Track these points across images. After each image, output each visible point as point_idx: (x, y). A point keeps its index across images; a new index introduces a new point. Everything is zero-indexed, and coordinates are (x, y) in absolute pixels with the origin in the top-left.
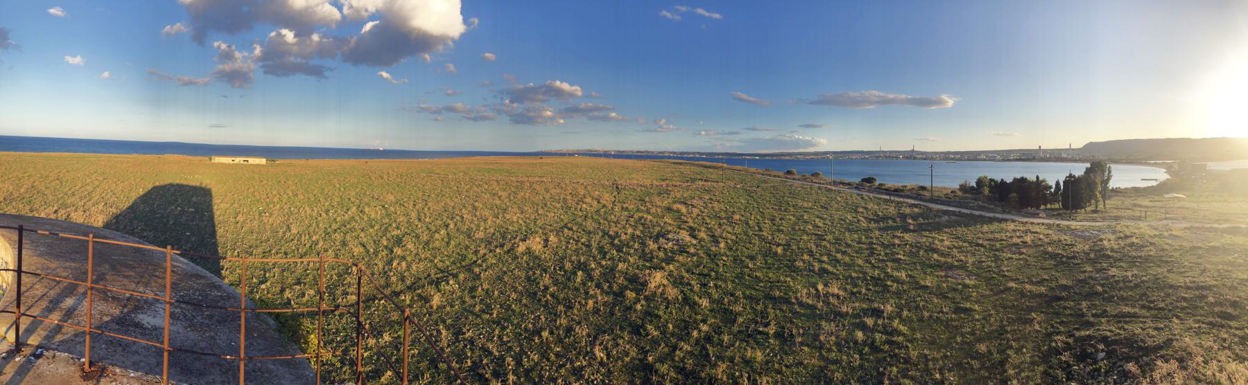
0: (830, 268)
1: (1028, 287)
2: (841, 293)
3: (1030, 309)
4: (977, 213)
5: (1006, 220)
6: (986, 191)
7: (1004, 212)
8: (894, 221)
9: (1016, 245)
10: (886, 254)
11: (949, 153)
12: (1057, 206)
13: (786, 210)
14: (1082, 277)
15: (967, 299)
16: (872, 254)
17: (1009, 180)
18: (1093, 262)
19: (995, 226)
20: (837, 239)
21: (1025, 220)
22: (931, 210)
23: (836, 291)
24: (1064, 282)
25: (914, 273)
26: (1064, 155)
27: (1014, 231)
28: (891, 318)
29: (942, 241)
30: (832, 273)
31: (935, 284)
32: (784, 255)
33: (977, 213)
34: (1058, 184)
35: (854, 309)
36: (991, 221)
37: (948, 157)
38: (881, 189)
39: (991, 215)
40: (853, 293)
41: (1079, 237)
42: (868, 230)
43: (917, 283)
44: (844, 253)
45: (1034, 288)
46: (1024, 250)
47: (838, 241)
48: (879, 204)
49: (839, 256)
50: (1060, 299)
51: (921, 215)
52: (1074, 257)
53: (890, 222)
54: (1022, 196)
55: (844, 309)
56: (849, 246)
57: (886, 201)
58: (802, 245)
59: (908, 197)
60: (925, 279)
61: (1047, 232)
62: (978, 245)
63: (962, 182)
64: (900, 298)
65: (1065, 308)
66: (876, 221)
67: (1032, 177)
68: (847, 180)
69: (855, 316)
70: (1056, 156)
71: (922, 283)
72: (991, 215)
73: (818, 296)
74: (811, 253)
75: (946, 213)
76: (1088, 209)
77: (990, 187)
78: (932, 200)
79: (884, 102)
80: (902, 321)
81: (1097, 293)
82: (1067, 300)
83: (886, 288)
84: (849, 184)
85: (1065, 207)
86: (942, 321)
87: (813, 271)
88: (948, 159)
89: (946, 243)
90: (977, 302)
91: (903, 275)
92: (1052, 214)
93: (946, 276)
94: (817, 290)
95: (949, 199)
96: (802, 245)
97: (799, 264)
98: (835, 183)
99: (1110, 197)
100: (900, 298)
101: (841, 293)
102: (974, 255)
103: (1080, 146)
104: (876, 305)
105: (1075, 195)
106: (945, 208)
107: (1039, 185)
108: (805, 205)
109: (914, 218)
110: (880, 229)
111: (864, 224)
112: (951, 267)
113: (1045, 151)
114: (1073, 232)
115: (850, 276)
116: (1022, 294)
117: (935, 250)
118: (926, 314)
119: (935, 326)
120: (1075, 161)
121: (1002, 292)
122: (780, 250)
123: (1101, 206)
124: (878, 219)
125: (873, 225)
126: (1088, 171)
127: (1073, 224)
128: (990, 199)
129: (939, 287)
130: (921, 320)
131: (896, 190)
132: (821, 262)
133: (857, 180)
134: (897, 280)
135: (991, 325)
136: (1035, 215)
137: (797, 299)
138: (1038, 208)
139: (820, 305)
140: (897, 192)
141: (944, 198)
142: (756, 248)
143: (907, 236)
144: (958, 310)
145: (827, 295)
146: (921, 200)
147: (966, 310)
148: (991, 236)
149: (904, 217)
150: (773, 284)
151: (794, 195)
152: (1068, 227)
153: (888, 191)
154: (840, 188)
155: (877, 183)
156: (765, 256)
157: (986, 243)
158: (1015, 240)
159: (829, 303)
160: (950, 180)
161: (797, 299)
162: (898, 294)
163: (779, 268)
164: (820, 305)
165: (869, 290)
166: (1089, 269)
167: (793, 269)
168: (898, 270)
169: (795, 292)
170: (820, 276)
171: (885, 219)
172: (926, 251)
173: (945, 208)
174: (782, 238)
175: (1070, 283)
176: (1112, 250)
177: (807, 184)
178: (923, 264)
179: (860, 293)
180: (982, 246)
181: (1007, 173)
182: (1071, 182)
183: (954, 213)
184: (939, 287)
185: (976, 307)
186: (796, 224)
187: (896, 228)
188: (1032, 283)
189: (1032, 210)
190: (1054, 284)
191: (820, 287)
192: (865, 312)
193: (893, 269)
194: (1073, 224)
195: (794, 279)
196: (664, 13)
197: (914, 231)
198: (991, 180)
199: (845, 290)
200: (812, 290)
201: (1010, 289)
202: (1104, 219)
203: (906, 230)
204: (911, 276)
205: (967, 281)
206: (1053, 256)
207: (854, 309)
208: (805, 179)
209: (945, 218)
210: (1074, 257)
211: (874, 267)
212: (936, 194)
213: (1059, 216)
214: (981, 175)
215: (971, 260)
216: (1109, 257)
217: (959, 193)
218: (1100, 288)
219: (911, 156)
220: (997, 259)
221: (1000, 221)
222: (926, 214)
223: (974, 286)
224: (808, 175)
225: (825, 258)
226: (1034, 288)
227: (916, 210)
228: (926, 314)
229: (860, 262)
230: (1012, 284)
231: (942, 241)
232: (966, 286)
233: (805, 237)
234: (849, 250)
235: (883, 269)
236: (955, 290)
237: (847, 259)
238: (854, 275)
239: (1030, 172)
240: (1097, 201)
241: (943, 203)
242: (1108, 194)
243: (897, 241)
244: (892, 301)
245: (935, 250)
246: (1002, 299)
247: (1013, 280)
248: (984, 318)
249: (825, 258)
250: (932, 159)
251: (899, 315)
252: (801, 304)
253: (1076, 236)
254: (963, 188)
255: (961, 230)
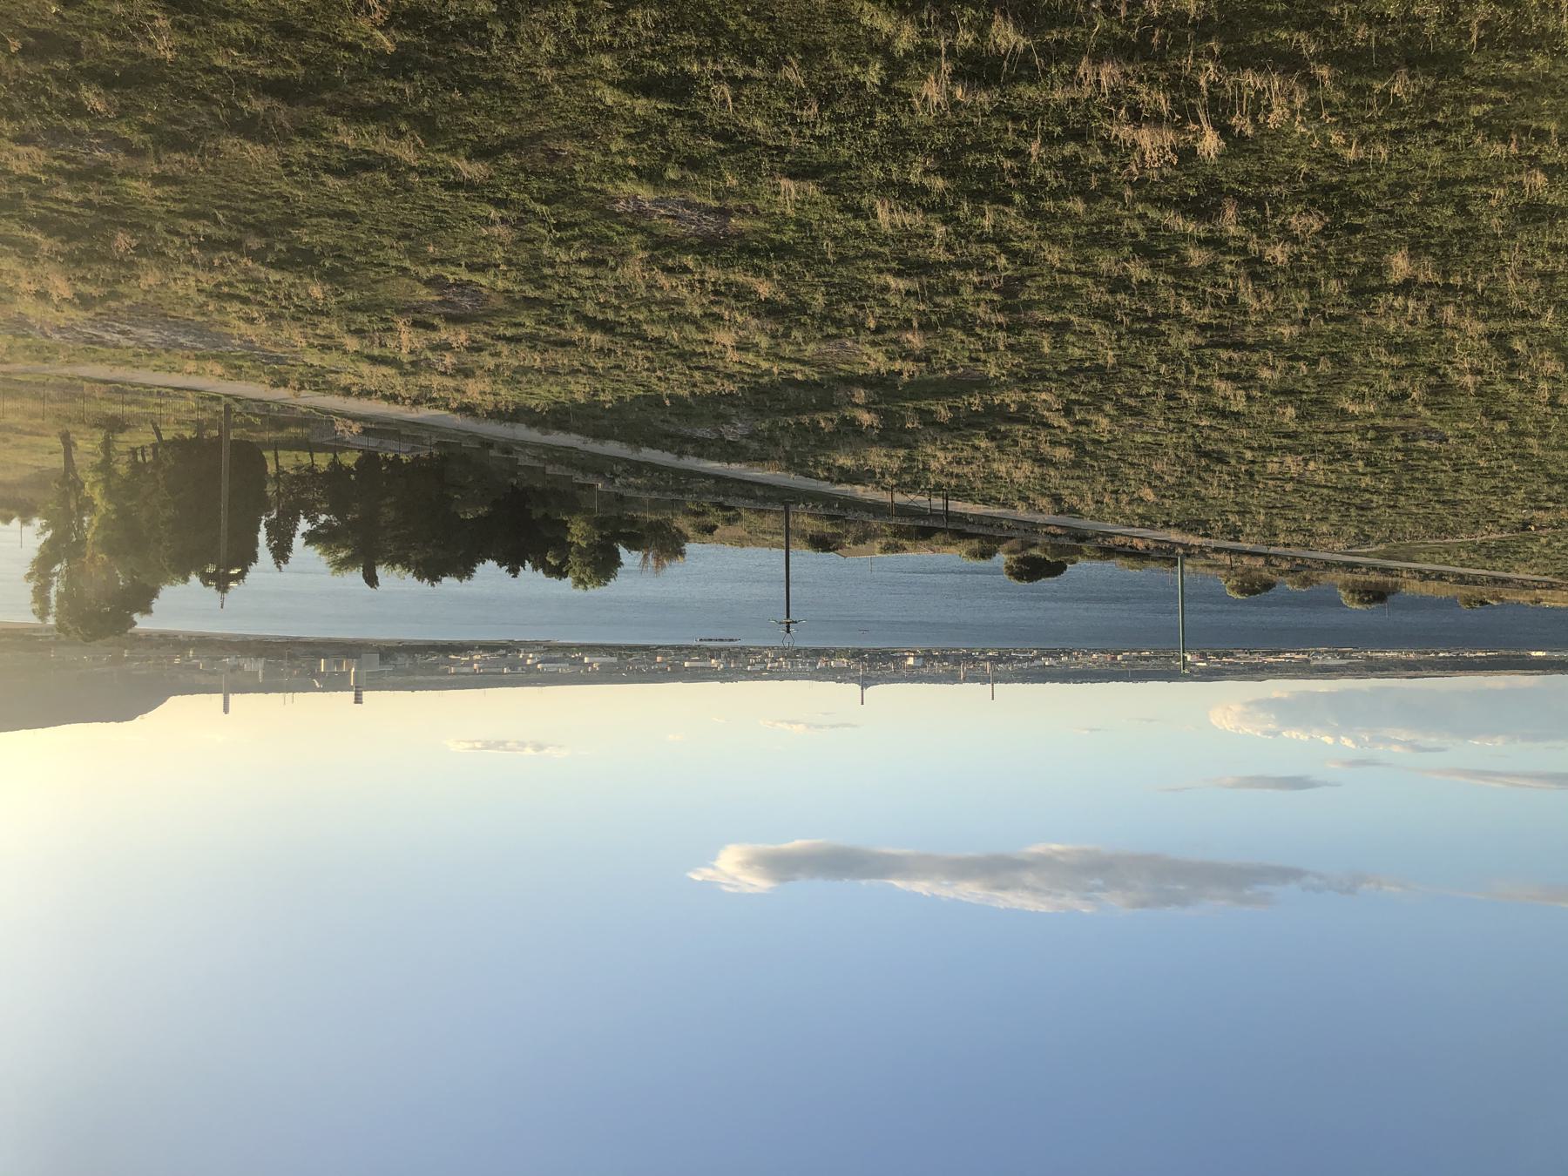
0: (1175, 221)
1: (406, 153)
2: (1125, 132)
3: (398, 65)
4: (613, 448)
5: (497, 415)
6: (578, 532)
7: (507, 447)
8: (927, 418)
9: (456, 319)
10: (953, 289)
11: (724, 676)
12: (289, 461)
13: (1382, 435)
14: (175, 162)
15: (643, 131)
16: (1009, 289)
17: (489, 572)
18: (121, 214)
19: (543, 395)
20: (1153, 335)
21: (424, 413)
22: (794, 463)
23: (1145, 138)
24: (255, 153)
25: (842, 223)
26: (255, 666)
27: (467, 373)
28: (925, 54)
29: (741, 347)
30: (1164, 203)
31: (764, 185)
32: (1378, 250)
33: (613, 448)
34: (281, 553)
35: (1071, 79)
36: (559, 417)
37: (729, 660)
38: (982, 537)
39: (558, 438)
40: (1079, 136)
41: (187, 326)
42: (1025, 380)
43: (832, 188)
44: (1120, 284)
45: (383, 145)
46: (424, 294)
47: (1149, 329)
48: (991, 478)
49: (1139, 271)
50: (280, 89)
51: (827, 442)
52: (210, 244)
53: (943, 414)
54: (453, 506)
55: (1109, 74)
56: (1104, 314)
57: (962, 493)
58: (1300, 301)
59: (877, 509)
60: (803, 203)
61: (331, 359)
62: (607, 327)
63: (675, 568)
64: (894, 128)
65: (250, 47)
66: (1001, 413)
67: (396, 581)
68: (1115, 568)
69: (1065, 52)
70: (295, 662)
71: (812, 189)
72: (558, 438)
73: (1220, 110)
74: (1257, 269)
75: (733, 452)
76: (143, 437)
77: (563, 547)
78: (785, 498)
79: (997, 868)
80: (883, 49)
81: (107, 82)
82: (242, 80)
83: (948, 163)
84: (1108, 552)
85: (248, 457)
86: (735, 48)
87: (1243, 201)
88: (734, 654)
89: (725, 338)
90: (606, 115)
91: (886, 216)
92: (313, 430)
93: (724, 213)
94: (1224, 131)
95: (724, 506)
96: (1300, 301)
97: (1306, 223)
98: (1167, 555)
99: (41, 480)
100: (894, 128)
101: (1125, 132)
102: (622, 290)
103: (176, 705)
104: (983, 97)
105: (206, 498)
106: (736, 469)
107: (362, 548)
108: (1292, 464)
109: (850, 432)
110: (983, 384)
111: (1045, 398)
112: (708, 247)
113: (334, 683)
114: (213, 346)
115: (1089, 197)
116: (427, 127)
117: (770, 309)
118: (793, 74)
119: (761, 30)
120: (203, 642)
121: (509, 145)
122: (1400, 265)
123: (88, 445)
124: (993, 421)
125: (1012, 398)
126: (143, 599)
127: (214, 380)
128: (570, 499)
129: (750, 173)
130: (812, 53)
131: (925, 534)
132: (1213, 242)
133: (1083, 569)
134: (908, 194)
135: (553, 26)
136: (377, 428)
137: (1311, 82)
138: (369, 460)
139: (1208, 74)
140: (922, 528)
141: (742, 504)
142: (1513, 258)
143: (875, 360)
144: (678, 88)
145: (1183, 116)
146: (828, 500)
147: (649, 87)
148: (561, 359)
149: (892, 435)
150: (1425, 118)
151: (1350, 502)
152: (237, 372)
153: (956, 529)
154: (1143, 537)
155: (1001, 559)
156: (1469, 235)
157: (579, 332)
158: (459, 336)
159: (1173, 85)
160: (722, 572)
161: (1311, 82)
162: (900, 144)
163: (1400, 189)
164: (1208, 74)
165: (1016, 153)
166: (140, 189)
167: (1334, 198)
168: (907, 235)
169: (1314, 109)
170: (1213, 187)
171: (963, 425)
172: (803, 308)
173: (736, 469)
174: (1396, 316)
175: (231, 144)
176: (28, 252)
177: (1286, 544)
178: (811, 258)
179: (1049, 140)
180: (592, 324)
181: (497, 595)
182: (225, 563)
183: (703, 448)
184: (750, 173)
185: (610, 97)
186: (1335, 383)
187: (918, 389)
188: (391, 165)
189: (390, 450)
190: (300, 150)
191: (1210, 143)
192: (1024, 68)
193: (927, 236)
194: (214, 380)
195: (1332, 158)
196: (482, 511)
197: (852, 381)
198: (558, 572)
199: (1108, 147)
200: (1241, 123)
201: (480, 153)
202: (71, 389)
203: (881, 384)
204: (858, 212)
205: (645, 193)
206: (300, 260)
207: (1071, 79)
208: (1299, 568)
209: (735, 431)
210: (210, 244)
211: (1000, 240)
212: (770, 522)
213: (278, 418)
214: (595, 592)
215: (633, 271)
216: (43, 224)
217: (682, 523)
218: (92, 97)
219: (873, 664)
220: (534, 271)
221: (519, 414)
222: (806, 448)
223: (618, 173)
224: (1289, 585)
225: (1197, 257)
226: (383, 145)
227: (846, 461)
228: (793, 74)
229: (1054, 255)
230: (473, 170)
231: (741, 347)
232: (651, 176)
233: (1287, 331)
234: (1100, 296)
235: (965, 233)
236: (693, 163)
237: (1106, 262)
238: (1078, 206)
239: (402, 601)
240: (105, 467)
241: (747, 488)
242: (51, 499)
243: (915, 340)
244: (922, 117)
245: (770, 309)
246: (509, 118)
247: (469, 186)
248: (580, 52)
249: (1197, 257)
250: (792, 654)
251: (895, 67)
252: (1291, 63)
253: (200, 331)
254: (667, 544)
255: (675, 383)
